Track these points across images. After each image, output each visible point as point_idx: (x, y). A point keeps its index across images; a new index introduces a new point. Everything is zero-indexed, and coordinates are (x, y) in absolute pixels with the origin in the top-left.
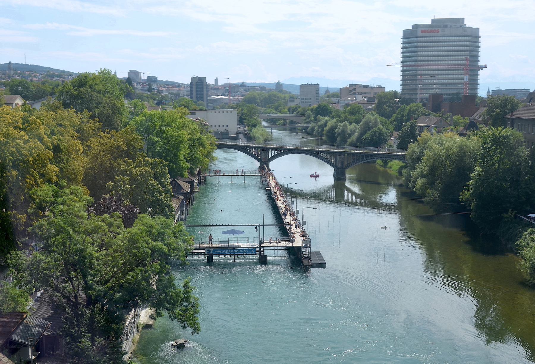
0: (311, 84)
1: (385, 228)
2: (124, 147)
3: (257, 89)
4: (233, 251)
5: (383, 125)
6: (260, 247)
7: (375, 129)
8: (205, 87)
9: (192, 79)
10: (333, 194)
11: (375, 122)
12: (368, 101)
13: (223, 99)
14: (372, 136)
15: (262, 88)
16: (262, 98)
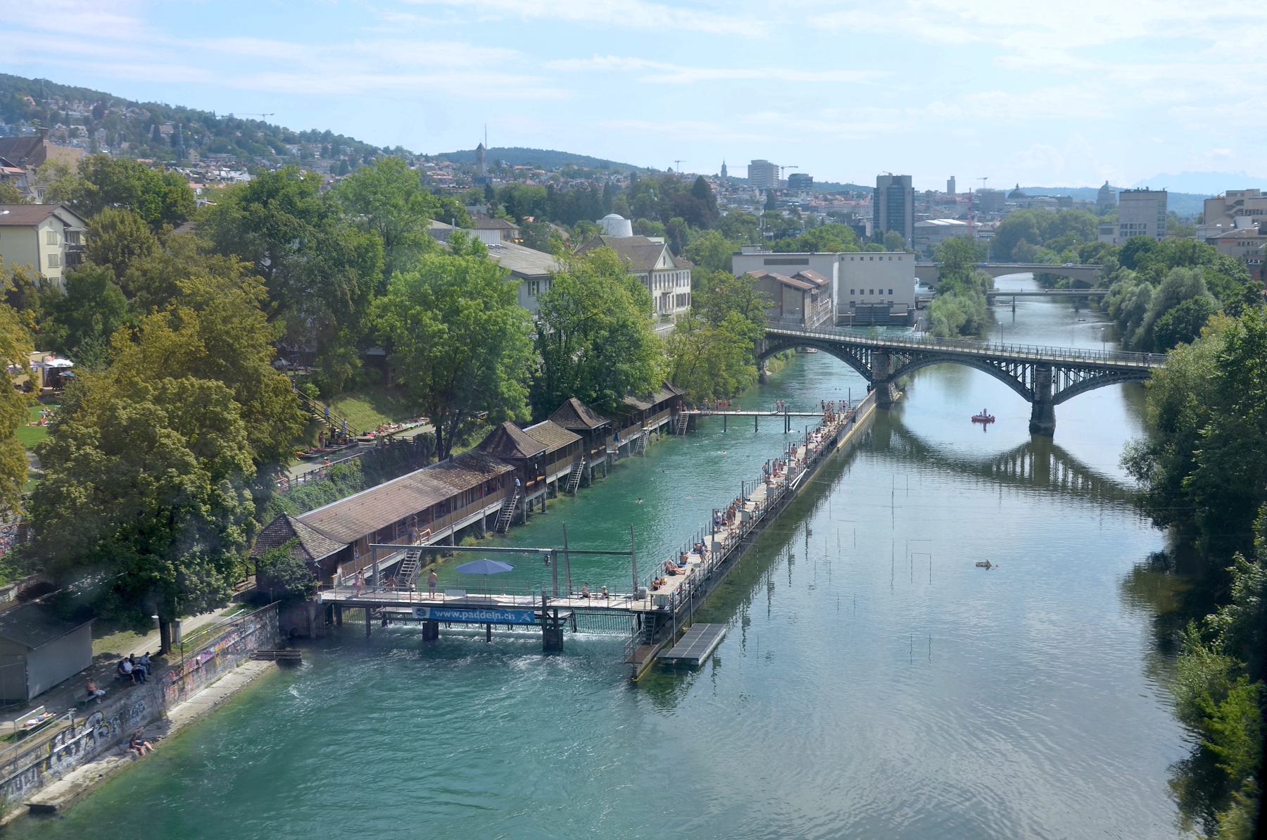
0: (1147, 191)
1: (987, 566)
2: (204, 352)
3: (1049, 204)
4: (485, 615)
5: (1216, 295)
6: (545, 608)
7: (1189, 303)
8: (908, 199)
9: (879, 178)
10: (1026, 466)
11: (1194, 285)
12: (1260, 232)
13: (952, 226)
14: (1178, 320)
15: (1064, 200)
16: (1044, 224)
